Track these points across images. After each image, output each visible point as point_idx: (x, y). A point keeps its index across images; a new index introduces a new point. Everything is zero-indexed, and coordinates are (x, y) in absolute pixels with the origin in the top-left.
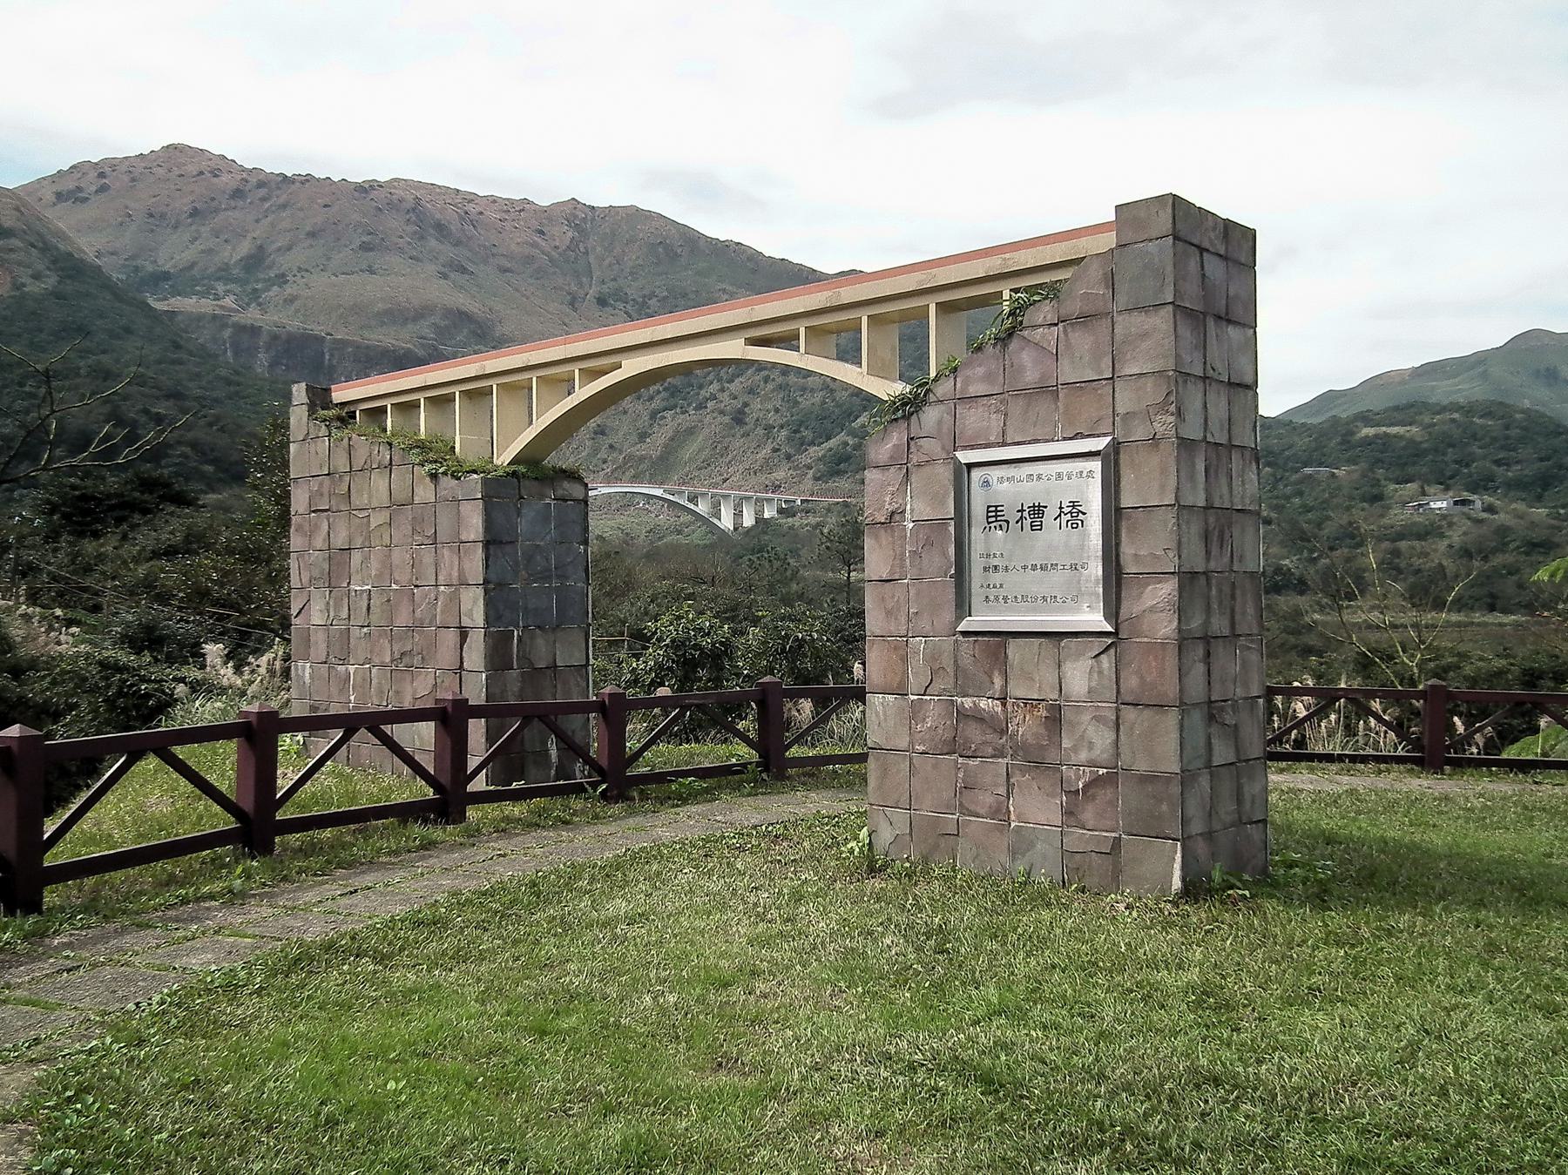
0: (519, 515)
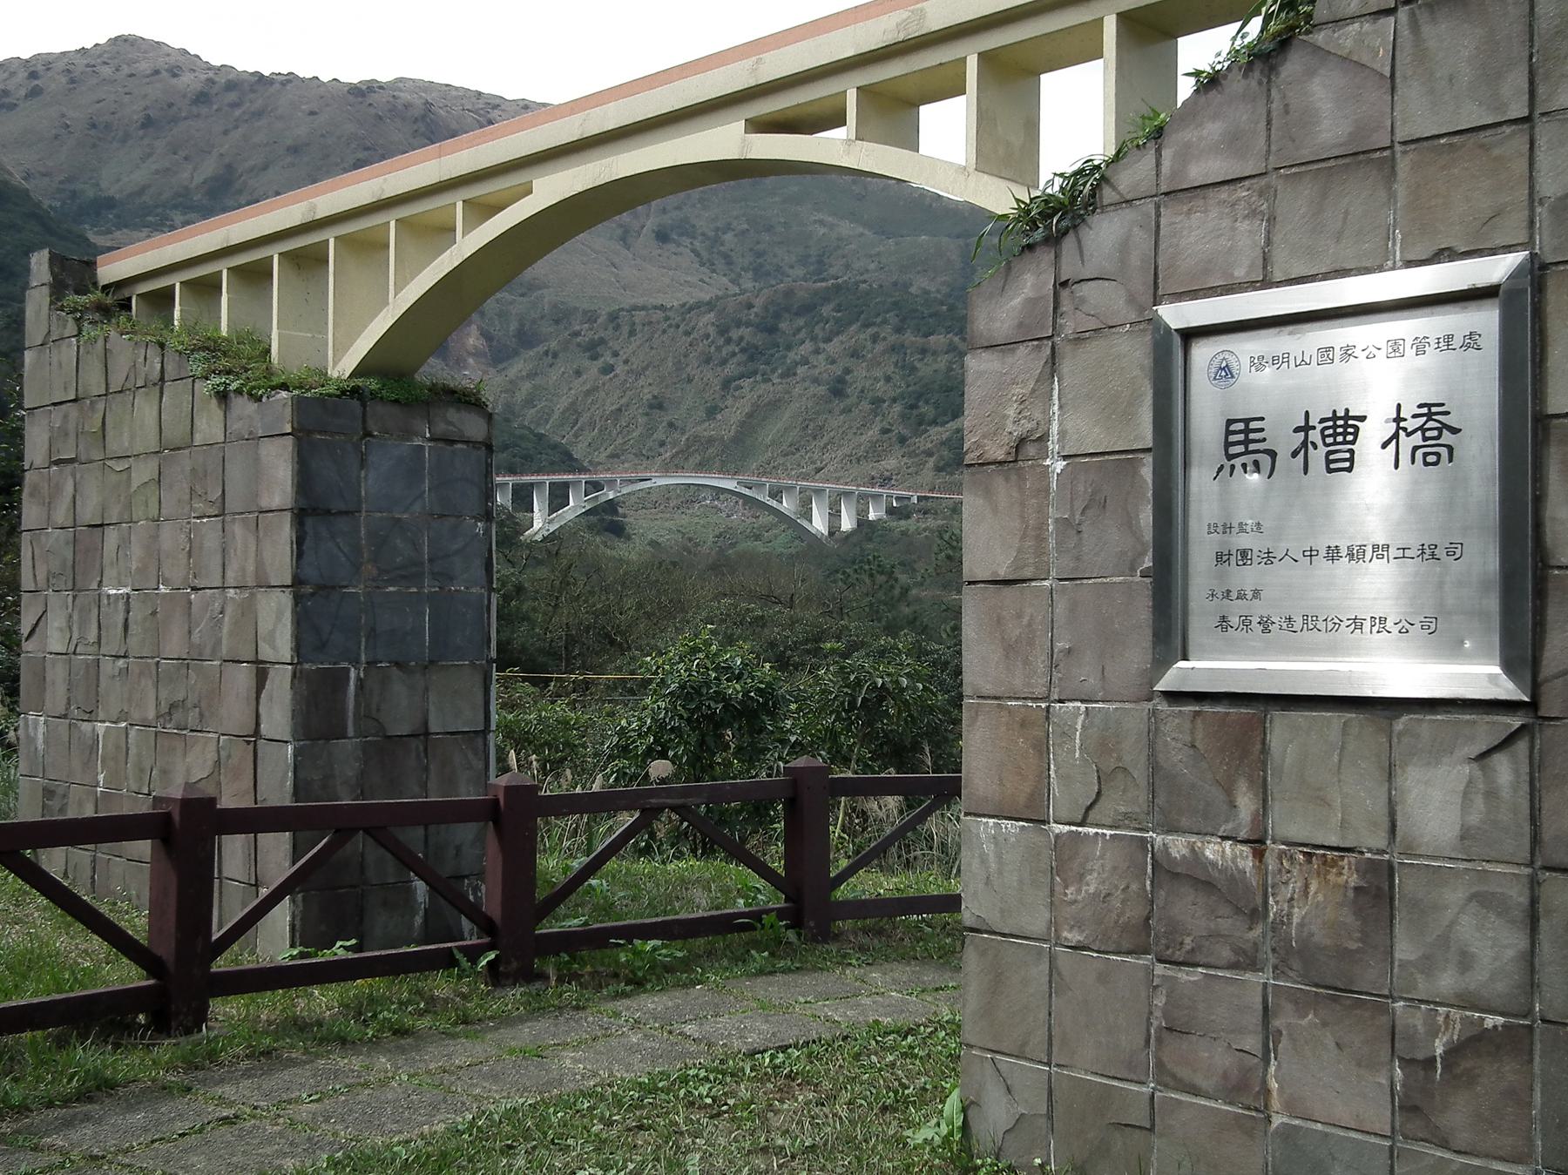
0: (363, 463)
